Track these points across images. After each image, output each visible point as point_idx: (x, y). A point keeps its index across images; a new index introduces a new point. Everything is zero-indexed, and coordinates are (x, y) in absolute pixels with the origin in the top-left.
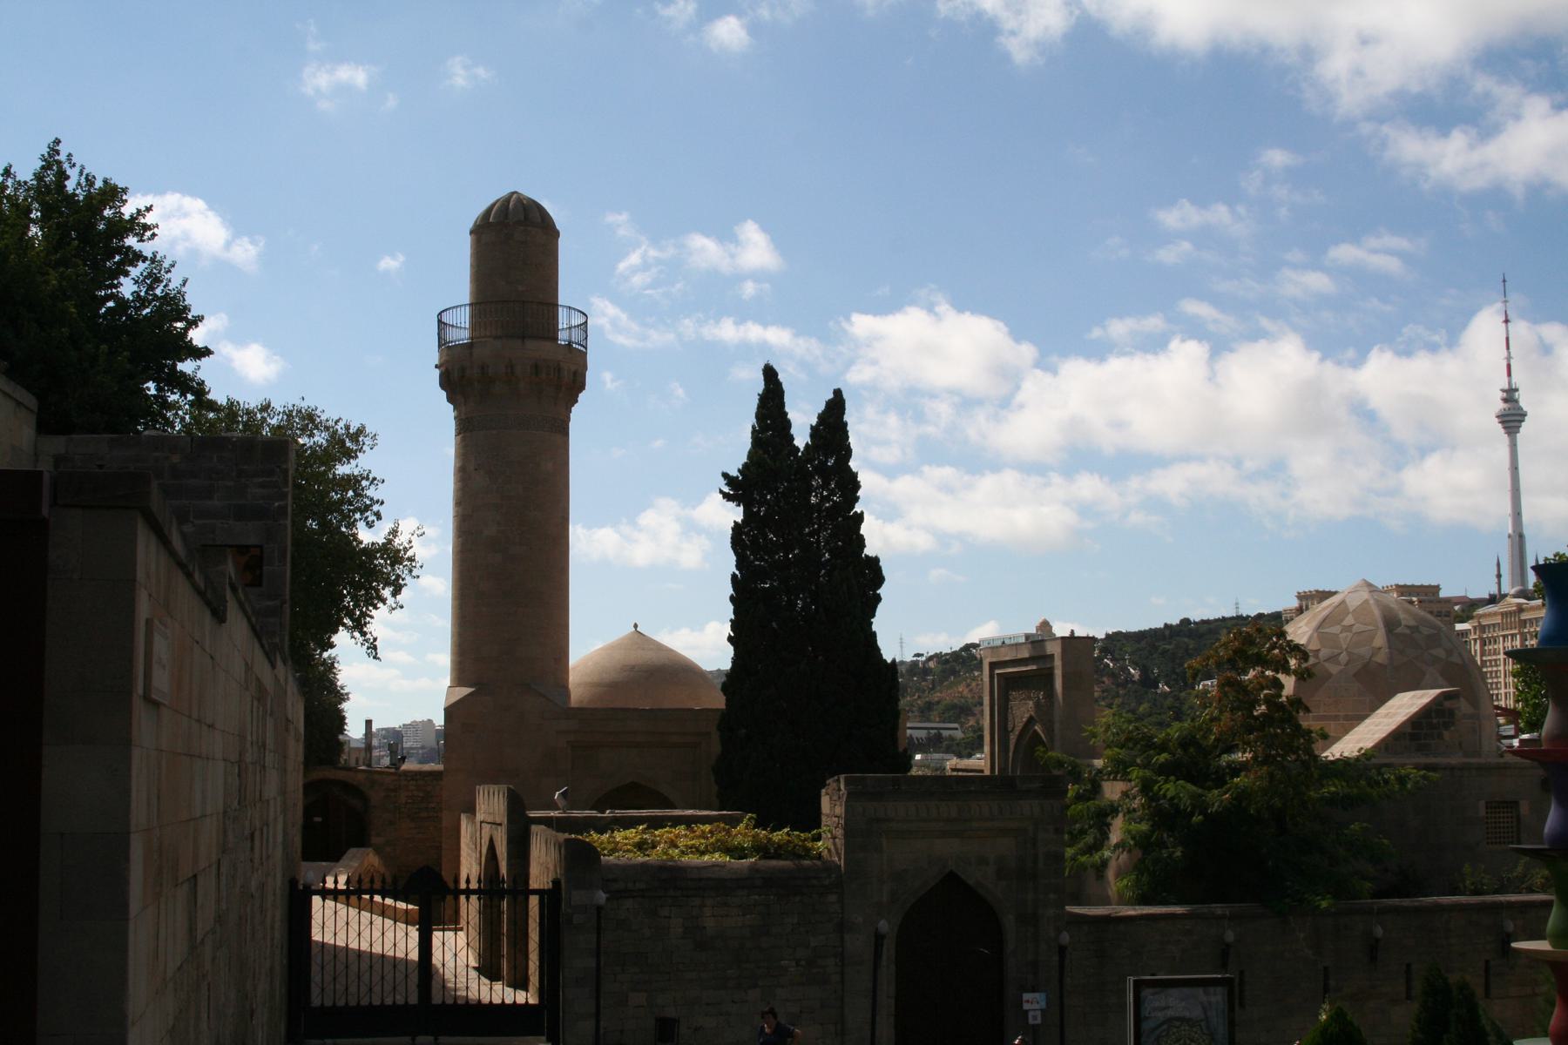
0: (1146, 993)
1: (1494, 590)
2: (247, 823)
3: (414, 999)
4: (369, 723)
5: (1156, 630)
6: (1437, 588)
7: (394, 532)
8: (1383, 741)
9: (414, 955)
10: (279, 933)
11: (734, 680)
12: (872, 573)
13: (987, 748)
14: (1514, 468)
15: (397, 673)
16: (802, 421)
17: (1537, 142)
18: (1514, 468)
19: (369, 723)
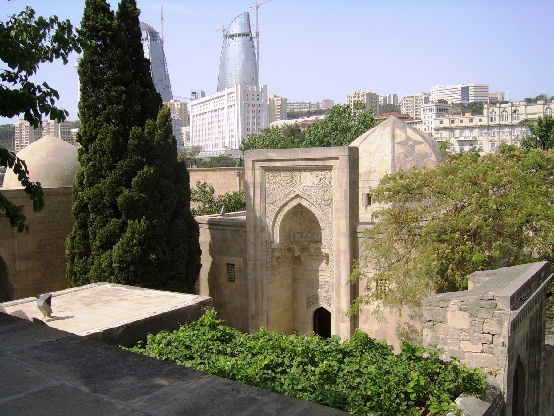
0: (247, 31)
1: (270, 175)
2: (105, 183)
3: (360, 221)
4: (66, 62)
5: (318, 241)
6: (119, 4)
7: (139, 222)
8: (96, 334)
9: (241, 38)
10: (296, 158)
11: (193, 218)
12: (201, 265)
13: (518, 311)
14: (162, 27)
15: (148, 170)
16: (45, 118)
17: (553, 170)
18: (162, 27)
19: (66, 62)
